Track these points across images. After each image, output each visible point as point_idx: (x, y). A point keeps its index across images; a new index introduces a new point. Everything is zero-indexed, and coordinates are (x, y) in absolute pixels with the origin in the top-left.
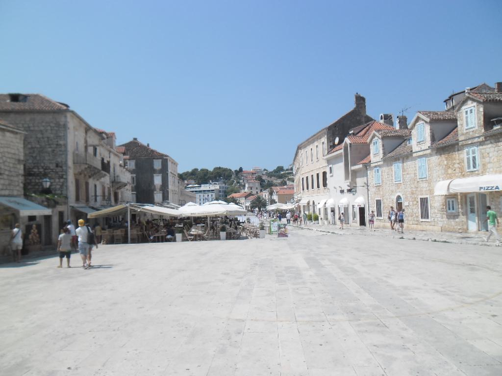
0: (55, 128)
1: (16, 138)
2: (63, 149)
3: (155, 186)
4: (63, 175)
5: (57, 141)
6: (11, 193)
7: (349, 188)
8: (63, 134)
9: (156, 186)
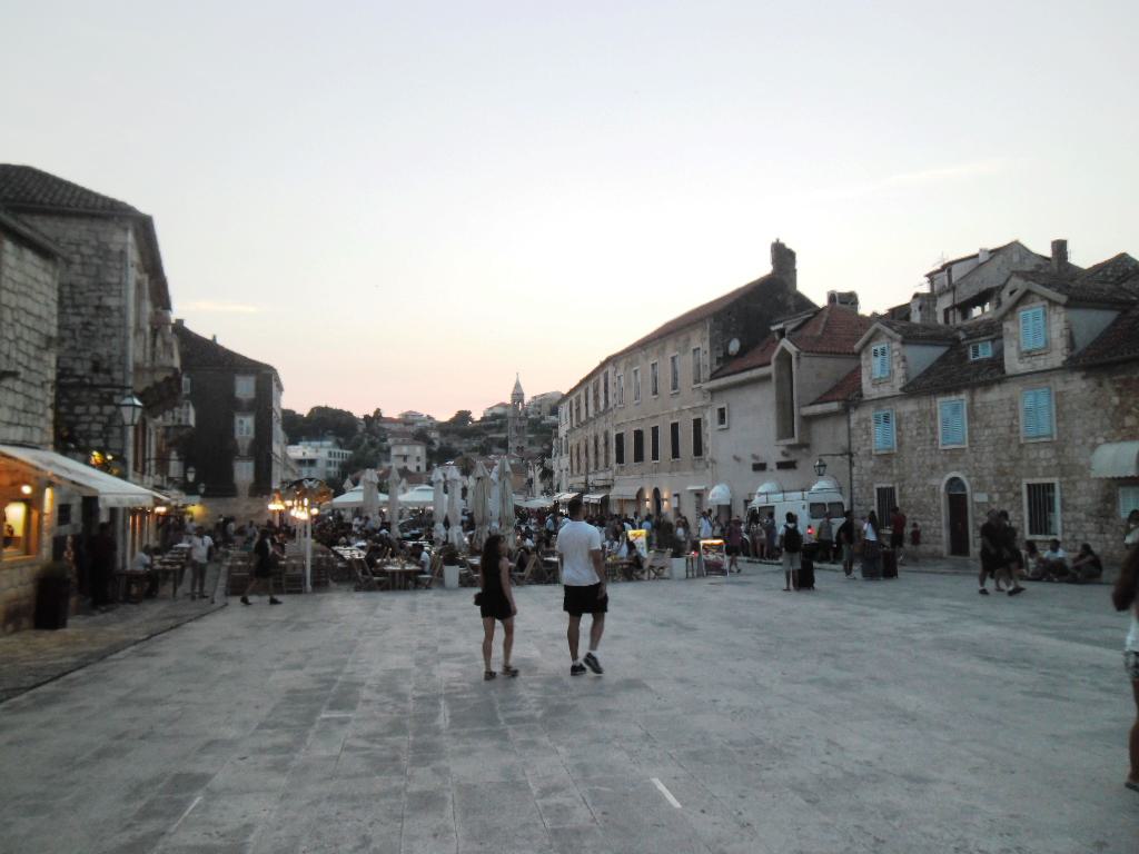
0: (96, 261)
1: (45, 270)
2: (115, 320)
3: (236, 442)
4: (111, 395)
5: (100, 298)
6: (28, 438)
7: (783, 459)
8: (115, 280)
9: (240, 444)
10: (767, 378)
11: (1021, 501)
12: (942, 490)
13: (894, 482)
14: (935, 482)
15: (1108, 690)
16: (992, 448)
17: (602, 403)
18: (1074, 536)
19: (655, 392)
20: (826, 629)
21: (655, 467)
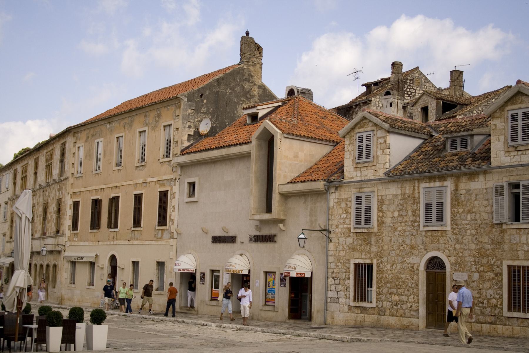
10: (247, 156)
11: (501, 281)
12: (422, 267)
13: (372, 259)
14: (414, 260)
15: (491, 323)
16: (473, 232)
17: (56, 172)
18: (383, 152)
19: (119, 164)
20: (306, 336)
21: (112, 235)
